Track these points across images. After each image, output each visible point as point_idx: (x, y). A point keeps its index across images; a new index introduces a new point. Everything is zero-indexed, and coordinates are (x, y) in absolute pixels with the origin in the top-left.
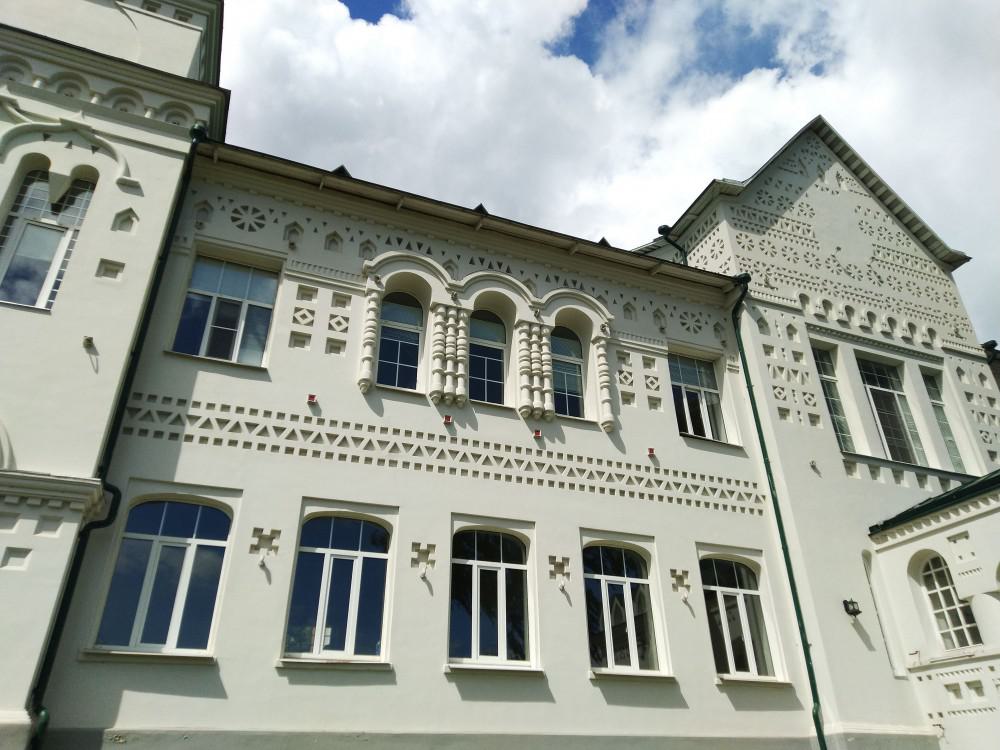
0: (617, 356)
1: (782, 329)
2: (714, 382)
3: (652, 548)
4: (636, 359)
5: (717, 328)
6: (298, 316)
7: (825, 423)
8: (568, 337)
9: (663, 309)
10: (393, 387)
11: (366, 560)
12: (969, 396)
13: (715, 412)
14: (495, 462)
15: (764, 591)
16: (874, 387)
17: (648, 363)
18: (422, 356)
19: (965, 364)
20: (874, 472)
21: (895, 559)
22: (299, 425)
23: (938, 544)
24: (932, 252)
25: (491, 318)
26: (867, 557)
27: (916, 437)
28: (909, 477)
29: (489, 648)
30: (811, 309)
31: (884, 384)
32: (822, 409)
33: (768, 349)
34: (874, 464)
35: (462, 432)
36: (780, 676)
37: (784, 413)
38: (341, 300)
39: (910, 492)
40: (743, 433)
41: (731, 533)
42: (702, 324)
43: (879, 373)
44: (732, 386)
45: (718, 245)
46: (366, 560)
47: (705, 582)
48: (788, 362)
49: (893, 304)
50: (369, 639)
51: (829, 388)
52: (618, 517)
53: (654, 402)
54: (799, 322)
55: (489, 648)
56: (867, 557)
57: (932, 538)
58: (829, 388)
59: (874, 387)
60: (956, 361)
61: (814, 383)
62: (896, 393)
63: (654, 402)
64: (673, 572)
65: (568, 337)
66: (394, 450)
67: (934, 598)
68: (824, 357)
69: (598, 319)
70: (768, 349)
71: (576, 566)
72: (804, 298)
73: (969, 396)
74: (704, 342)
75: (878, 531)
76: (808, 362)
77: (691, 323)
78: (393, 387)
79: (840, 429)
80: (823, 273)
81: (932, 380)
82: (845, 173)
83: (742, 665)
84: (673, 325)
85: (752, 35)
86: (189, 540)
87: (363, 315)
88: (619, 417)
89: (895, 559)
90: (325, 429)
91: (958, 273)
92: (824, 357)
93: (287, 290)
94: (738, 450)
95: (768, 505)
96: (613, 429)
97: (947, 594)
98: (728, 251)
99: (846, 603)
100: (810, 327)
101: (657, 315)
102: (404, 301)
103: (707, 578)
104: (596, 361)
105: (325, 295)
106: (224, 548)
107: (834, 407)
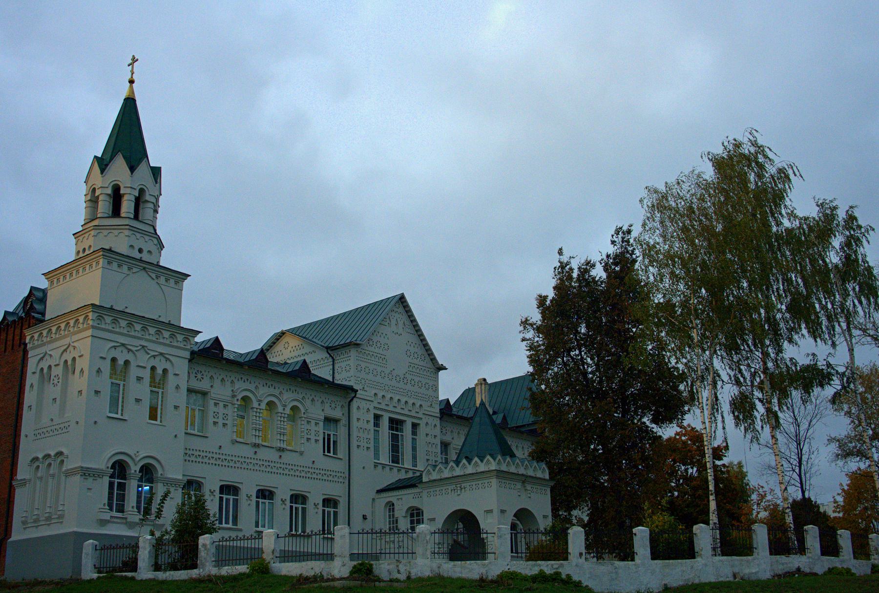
5: (342, 406)
9: (225, 378)
10: (398, 465)
11: (233, 499)
16: (393, 432)
23: (394, 500)
24: (433, 364)
26: (373, 499)
29: (227, 522)
31: (397, 430)
34: (384, 466)
37: (358, 446)
39: (392, 477)
42: (337, 406)
43: (396, 424)
45: (375, 373)
46: (233, 499)
47: (220, 493)
49: (387, 388)
50: (235, 522)
53: (316, 441)
55: (227, 522)
57: (392, 496)
59: (393, 432)
61: (371, 436)
62: (400, 433)
64: (282, 499)
67: (389, 515)
75: (379, 492)
77: (199, 376)
78: (398, 465)
81: (415, 426)
85: (550, 298)
91: (441, 373)
92: (377, 417)
97: (393, 515)
99: (363, 516)
103: (221, 492)
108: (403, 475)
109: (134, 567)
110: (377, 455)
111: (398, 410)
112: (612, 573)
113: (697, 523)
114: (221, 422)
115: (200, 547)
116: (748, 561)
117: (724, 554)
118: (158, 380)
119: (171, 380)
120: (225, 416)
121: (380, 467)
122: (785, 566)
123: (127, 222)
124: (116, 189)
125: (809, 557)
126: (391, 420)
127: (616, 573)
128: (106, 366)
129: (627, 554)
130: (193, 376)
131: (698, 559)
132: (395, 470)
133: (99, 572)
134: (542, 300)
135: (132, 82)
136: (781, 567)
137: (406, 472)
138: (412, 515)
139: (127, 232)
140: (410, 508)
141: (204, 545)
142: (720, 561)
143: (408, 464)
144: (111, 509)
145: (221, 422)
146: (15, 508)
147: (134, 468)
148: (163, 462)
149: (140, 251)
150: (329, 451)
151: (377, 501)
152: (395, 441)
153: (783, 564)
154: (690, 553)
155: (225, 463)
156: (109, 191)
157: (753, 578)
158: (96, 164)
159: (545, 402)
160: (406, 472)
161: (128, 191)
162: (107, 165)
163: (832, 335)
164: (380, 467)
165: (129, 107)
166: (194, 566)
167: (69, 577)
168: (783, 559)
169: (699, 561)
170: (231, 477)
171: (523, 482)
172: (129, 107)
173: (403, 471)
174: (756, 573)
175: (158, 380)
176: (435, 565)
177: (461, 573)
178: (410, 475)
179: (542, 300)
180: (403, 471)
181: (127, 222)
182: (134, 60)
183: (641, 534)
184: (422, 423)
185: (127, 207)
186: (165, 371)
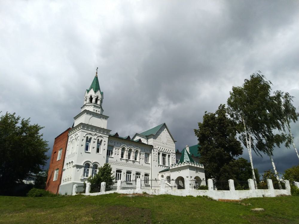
0: (140, 154)
1: (156, 151)
2: (149, 156)
3: (132, 172)
4: (142, 154)
5: (150, 150)
6: (116, 152)
7: (157, 162)
8: (137, 152)
12: (172, 158)
13: (148, 159)
14: (130, 165)
15: (149, 177)
17: (143, 155)
18: (89, 187)
19: (173, 154)
20: (163, 167)
21: (160, 175)
22: (116, 162)
23: (163, 174)
25: (130, 150)
26: (158, 174)
27: (166, 162)
28: (165, 166)
30: (159, 149)
32: (157, 160)
33: (154, 154)
34: (161, 166)
35: (127, 162)
36: (149, 184)
37: (154, 160)
38: (118, 150)
39: (164, 168)
40: (150, 162)
41: (147, 172)
43: (164, 155)
44: (150, 156)
48: (155, 155)
51: (159, 157)
52: (139, 170)
53: (143, 159)
54: (157, 150)
56: (158, 174)
57: (163, 174)
58: (159, 157)
60: (172, 154)
61: (157, 157)
63: (143, 159)
65: (137, 152)
66: (122, 164)
68: (159, 154)
69: (139, 151)
70: (154, 154)
71: (135, 175)
72: (158, 147)
73: (172, 158)
74: (148, 152)
75: (160, 172)
76: (157, 155)
79: (159, 161)
80: (161, 144)
81: (169, 156)
82: (166, 130)
83: (146, 183)
84: (146, 151)
86: (239, 185)
87: (120, 151)
88: (91, 175)
89: (160, 175)
90: (117, 163)
92: (159, 154)
93: (114, 149)
94: (149, 164)
95: (151, 169)
96: (139, 162)
98: (152, 142)
100: (158, 151)
101: (144, 149)
102: (123, 149)
104: (138, 154)
105: (117, 149)
106: (228, 189)
107: (159, 159)
108: (166, 168)
109: (84, 192)
110: (159, 163)
111: (165, 151)
112: (222, 194)
113: (249, 179)
114: (117, 153)
115: (101, 185)
116: (267, 191)
117: (258, 189)
118: (99, 143)
119: (103, 143)
120: (118, 152)
121: (160, 166)
122: (279, 193)
123: (93, 104)
124: (91, 96)
125: (287, 190)
126: (163, 154)
127: (224, 194)
128: (85, 139)
129: (228, 189)
130: (110, 142)
131: (251, 190)
132: (164, 167)
133: (77, 193)
134: (199, 124)
135: (97, 73)
136: (278, 193)
137: (167, 167)
138: (168, 178)
139: (93, 106)
140: (167, 176)
141: (102, 185)
142: (257, 191)
143: (167, 165)
144: (84, 176)
145: (117, 153)
146: (233, 199)
147: (91, 165)
148: (99, 163)
149: (96, 111)
150: (146, 162)
151: (159, 175)
152: (164, 159)
153: (279, 192)
154: (247, 188)
155: (118, 164)
156: (89, 97)
157: (269, 197)
158: (87, 91)
159: (187, 215)
160: (167, 167)
161: (94, 97)
162: (89, 91)
163: (284, 128)
164: (160, 166)
165: (96, 78)
166: (99, 191)
167: (70, 195)
168: (278, 190)
169: (250, 191)
170: (119, 168)
171: (197, 169)
172: (96, 78)
173: (166, 167)
174: (270, 195)
175: (99, 143)
176: (166, 191)
177: (174, 193)
178: (168, 168)
179: (199, 124)
180: (166, 167)
181: (93, 104)
182: (97, 68)
183: (231, 182)
184: (171, 155)
185: (94, 101)
186: (102, 140)
